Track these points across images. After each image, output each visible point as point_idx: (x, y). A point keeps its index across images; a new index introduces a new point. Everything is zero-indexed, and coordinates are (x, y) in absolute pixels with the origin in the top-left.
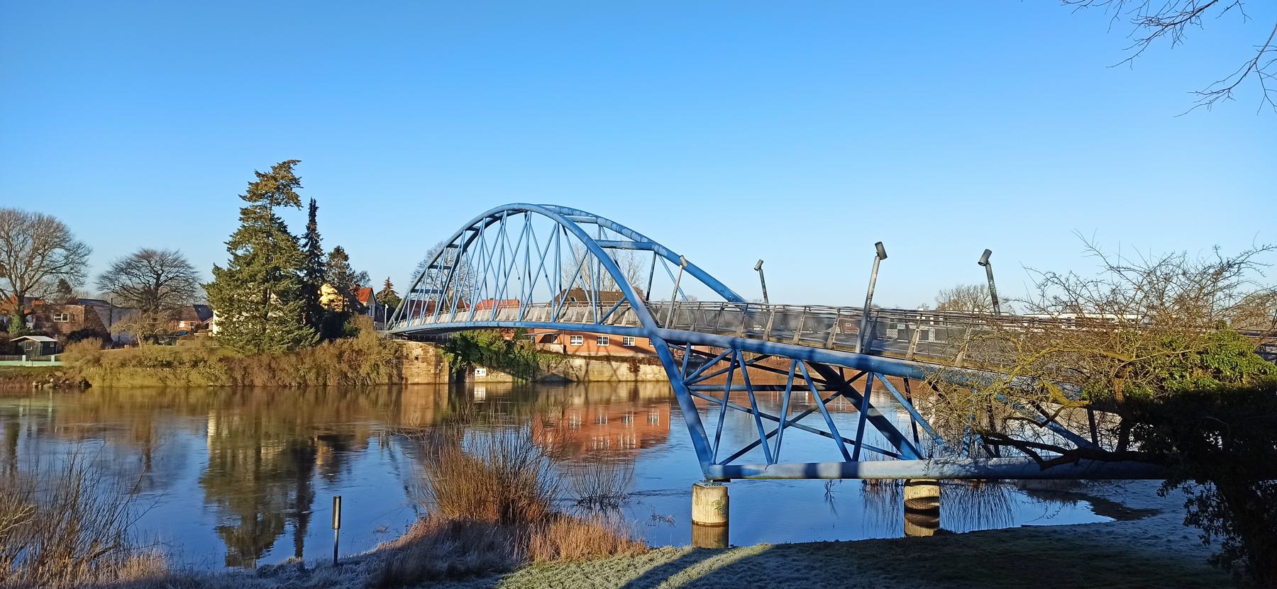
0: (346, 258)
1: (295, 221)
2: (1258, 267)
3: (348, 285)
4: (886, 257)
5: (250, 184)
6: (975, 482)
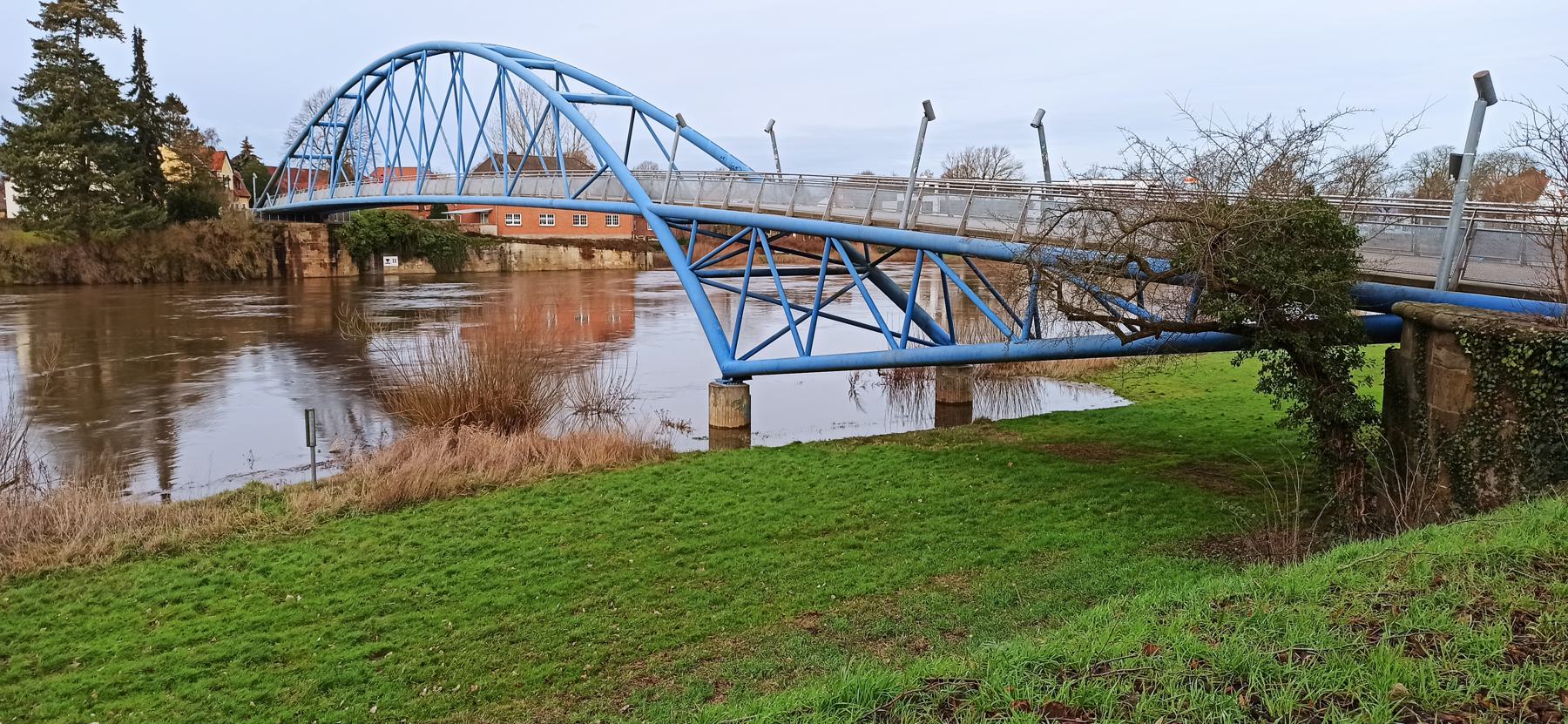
0: (184, 111)
1: (113, 57)
2: (1339, 131)
3: (194, 147)
4: (934, 118)
5: (43, 4)
6: (1136, 330)
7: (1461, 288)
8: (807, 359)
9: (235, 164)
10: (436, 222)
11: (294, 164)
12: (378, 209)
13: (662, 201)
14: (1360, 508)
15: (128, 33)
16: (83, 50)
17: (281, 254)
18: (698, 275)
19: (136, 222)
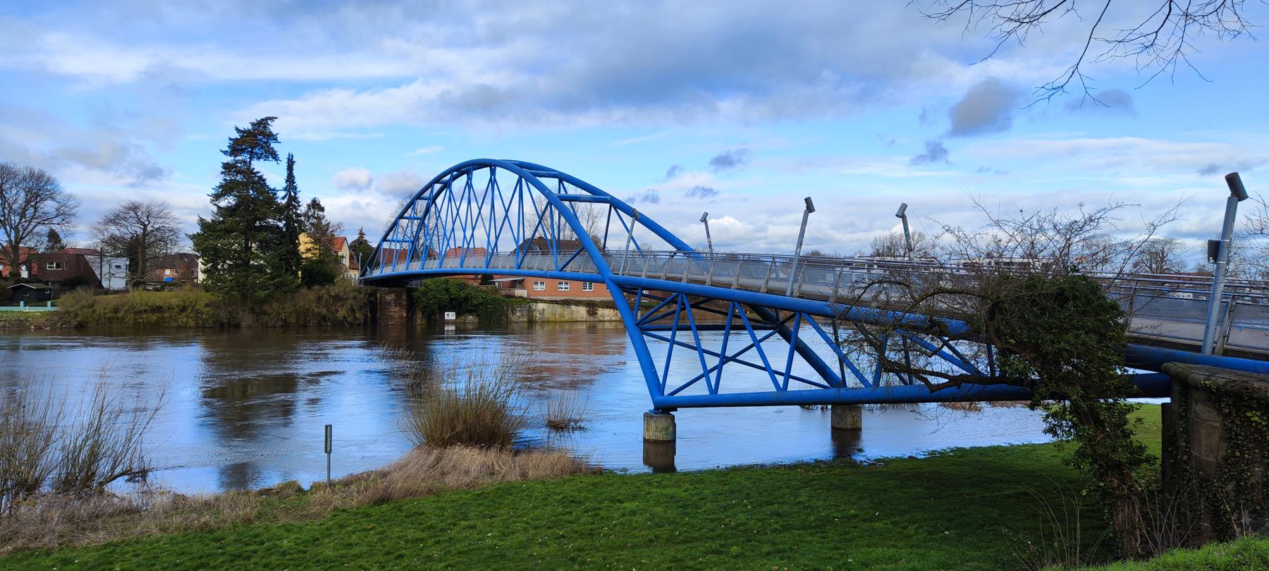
0: (322, 209)
1: (272, 174)
3: (323, 234)
4: (814, 210)
7: (1226, 352)
8: (714, 396)
9: (353, 247)
10: (484, 288)
11: (386, 245)
12: (443, 278)
13: (620, 273)
14: (1136, 540)
15: (283, 157)
16: (253, 169)
17: (374, 311)
18: (641, 329)
19: (278, 287)
